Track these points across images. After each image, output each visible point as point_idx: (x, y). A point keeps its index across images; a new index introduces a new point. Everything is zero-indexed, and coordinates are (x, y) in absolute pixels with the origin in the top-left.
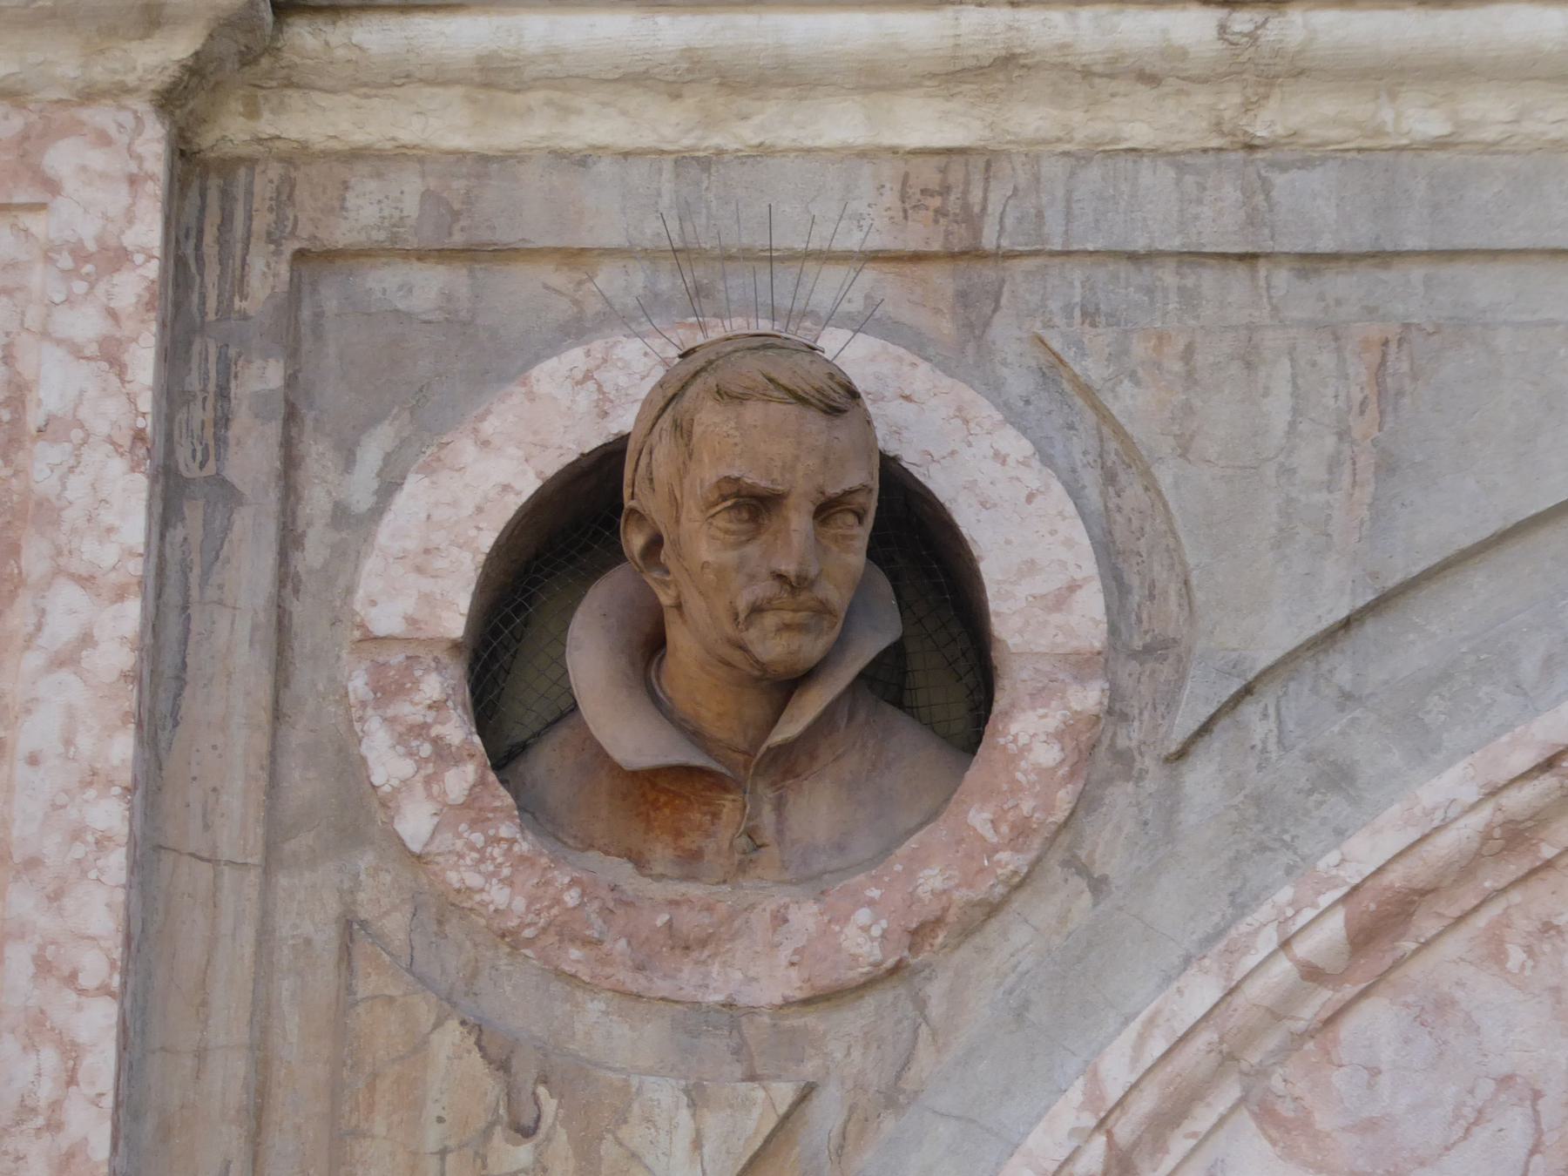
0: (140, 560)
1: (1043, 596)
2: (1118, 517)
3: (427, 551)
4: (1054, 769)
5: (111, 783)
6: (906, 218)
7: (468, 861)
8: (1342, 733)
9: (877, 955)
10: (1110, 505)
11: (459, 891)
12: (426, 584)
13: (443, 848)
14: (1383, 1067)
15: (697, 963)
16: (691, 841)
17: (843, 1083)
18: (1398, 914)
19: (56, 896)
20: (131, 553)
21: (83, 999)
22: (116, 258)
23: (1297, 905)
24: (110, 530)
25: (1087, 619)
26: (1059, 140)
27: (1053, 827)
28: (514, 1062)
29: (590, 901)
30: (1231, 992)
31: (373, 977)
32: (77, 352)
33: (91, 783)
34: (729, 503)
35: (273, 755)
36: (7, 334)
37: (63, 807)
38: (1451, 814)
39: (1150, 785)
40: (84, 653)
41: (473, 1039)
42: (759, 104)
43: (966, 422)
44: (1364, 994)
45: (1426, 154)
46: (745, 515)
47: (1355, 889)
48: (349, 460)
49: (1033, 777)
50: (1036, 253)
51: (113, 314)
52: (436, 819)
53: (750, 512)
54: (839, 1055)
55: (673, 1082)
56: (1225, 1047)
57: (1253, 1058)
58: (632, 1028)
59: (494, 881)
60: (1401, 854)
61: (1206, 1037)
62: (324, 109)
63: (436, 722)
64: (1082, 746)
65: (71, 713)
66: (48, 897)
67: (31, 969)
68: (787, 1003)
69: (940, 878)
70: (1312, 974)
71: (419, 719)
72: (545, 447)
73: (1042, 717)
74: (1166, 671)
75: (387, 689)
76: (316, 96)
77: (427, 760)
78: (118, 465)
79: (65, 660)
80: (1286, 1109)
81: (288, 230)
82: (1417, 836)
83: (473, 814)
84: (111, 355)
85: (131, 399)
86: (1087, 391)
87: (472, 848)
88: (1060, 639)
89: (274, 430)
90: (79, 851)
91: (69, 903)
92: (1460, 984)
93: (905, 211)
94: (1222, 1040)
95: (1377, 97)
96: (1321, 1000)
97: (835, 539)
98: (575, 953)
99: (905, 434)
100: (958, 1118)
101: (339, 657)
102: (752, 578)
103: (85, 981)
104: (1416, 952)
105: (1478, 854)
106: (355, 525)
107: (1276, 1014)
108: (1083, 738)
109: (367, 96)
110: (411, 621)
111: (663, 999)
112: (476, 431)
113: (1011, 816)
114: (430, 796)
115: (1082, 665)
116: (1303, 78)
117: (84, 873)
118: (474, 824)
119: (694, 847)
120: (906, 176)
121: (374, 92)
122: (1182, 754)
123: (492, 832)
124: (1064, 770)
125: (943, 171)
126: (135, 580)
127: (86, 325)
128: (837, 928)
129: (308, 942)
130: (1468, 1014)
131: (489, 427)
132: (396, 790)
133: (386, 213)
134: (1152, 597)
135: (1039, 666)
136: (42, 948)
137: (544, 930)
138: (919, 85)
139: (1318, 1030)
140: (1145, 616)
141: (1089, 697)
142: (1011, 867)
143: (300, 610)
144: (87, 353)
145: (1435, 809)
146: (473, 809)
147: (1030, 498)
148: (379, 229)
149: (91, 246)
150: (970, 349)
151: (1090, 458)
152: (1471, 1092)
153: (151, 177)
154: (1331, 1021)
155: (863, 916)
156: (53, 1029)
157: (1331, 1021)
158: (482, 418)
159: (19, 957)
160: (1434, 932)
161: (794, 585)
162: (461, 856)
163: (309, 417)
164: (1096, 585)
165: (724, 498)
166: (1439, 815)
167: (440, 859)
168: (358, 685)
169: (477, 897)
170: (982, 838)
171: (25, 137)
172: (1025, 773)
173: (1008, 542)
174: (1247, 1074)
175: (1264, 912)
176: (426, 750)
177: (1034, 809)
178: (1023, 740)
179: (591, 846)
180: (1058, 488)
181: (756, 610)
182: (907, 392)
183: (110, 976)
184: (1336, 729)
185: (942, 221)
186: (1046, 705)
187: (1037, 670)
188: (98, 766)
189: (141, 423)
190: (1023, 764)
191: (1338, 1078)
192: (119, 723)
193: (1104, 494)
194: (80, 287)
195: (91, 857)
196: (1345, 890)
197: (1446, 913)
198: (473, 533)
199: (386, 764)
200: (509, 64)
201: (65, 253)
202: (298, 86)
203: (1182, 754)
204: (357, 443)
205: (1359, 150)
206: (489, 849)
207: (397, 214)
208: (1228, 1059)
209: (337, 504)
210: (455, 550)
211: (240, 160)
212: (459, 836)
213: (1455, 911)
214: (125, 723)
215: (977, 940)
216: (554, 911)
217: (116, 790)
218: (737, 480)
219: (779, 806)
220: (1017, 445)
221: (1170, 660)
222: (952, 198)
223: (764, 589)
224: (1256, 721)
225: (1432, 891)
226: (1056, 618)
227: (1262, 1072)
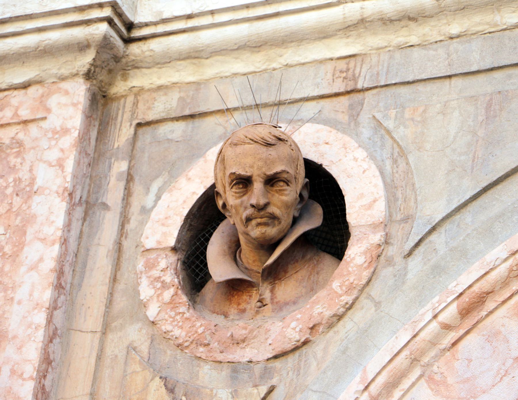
0: (61, 231)
1: (365, 205)
2: (397, 175)
3: (166, 218)
4: (362, 265)
5: (43, 307)
6: (333, 82)
7: (169, 322)
8: (464, 240)
9: (298, 338)
10: (394, 171)
11: (165, 333)
12: (165, 229)
13: (161, 318)
14: (473, 359)
15: (241, 348)
16: (243, 306)
17: (285, 385)
18: (478, 302)
19: (20, 348)
20: (58, 229)
21: (24, 382)
22: (65, 131)
23: (439, 302)
24: (53, 222)
25: (379, 211)
26: (386, 47)
27: (362, 286)
28: (176, 389)
29: (208, 330)
30: (415, 336)
31: (133, 365)
32: (50, 165)
33: (36, 308)
34: (234, 182)
35: (111, 294)
36: (32, 162)
37: (26, 317)
38: (497, 263)
39: (397, 267)
40: (40, 264)
41: (163, 383)
42: (285, 50)
43: (346, 148)
44: (467, 333)
45: (514, 30)
46: (241, 186)
47: (461, 294)
48: (148, 190)
49: (355, 269)
50: (376, 87)
51: (62, 150)
52: (160, 309)
53: (243, 185)
54: (285, 375)
55: (227, 390)
56: (413, 357)
57: (426, 360)
58: (218, 373)
59: (176, 327)
60: (478, 280)
61: (405, 353)
62: (146, 74)
63: (164, 276)
64: (373, 256)
65: (33, 285)
66: (18, 349)
67: (9, 373)
68: (268, 360)
69: (321, 308)
70: (447, 327)
71: (158, 275)
72: (208, 177)
73: (360, 247)
74: (407, 226)
75: (150, 266)
76: (144, 70)
77: (159, 289)
78: (58, 200)
79: (33, 268)
80: (437, 377)
81: (135, 117)
82: (483, 272)
83: (172, 306)
84: (60, 164)
85: (65, 178)
86: (388, 132)
87: (171, 317)
88: (369, 219)
89: (122, 185)
90: (29, 331)
91: (24, 349)
92: (503, 325)
93: (333, 80)
94: (411, 354)
95: (494, 12)
96: (452, 336)
97: (277, 191)
98: (201, 349)
99: (325, 156)
100: (319, 392)
101: (137, 258)
102: (246, 208)
103: (25, 376)
104: (487, 316)
105: (508, 277)
106: (145, 211)
107: (433, 343)
108: (374, 253)
109: (160, 68)
110: (159, 242)
111: (228, 362)
112: (187, 175)
113: (347, 283)
114: (158, 301)
115: (374, 227)
116: (466, 10)
117: (30, 338)
118: (172, 309)
119: (243, 308)
120: (335, 67)
121: (162, 66)
122: (410, 254)
123: (177, 311)
124: (366, 264)
125: (348, 64)
126: (58, 238)
127: (53, 155)
128: (285, 330)
129: (116, 356)
130: (505, 336)
131: (190, 174)
132: (148, 300)
133: (166, 107)
134: (405, 201)
135: (361, 230)
136: (13, 366)
137: (192, 343)
138: (336, 35)
139: (450, 348)
140: (402, 208)
141: (377, 238)
142: (345, 301)
143: (126, 244)
144: (53, 164)
145: (491, 262)
146: (172, 304)
147: (364, 172)
148: (163, 112)
149: (58, 129)
150: (352, 124)
151: (389, 156)
152: (504, 364)
153: (80, 103)
154: (454, 344)
155: (293, 324)
156: (13, 393)
157: (454, 344)
158: (189, 171)
159: (6, 370)
160: (493, 307)
161: (260, 208)
162: (167, 320)
163: (137, 178)
164: (383, 199)
165: (233, 181)
166: (492, 264)
167: (160, 322)
168: (140, 266)
169: (171, 334)
170: (336, 292)
171: (43, 96)
172: (352, 267)
173: (355, 188)
174: (424, 366)
175: (429, 306)
176: (159, 285)
177: (354, 280)
178: (352, 256)
179: (214, 313)
180: (374, 167)
181: (249, 220)
182: (327, 142)
183: (33, 373)
184: (461, 238)
185: (345, 80)
186: (362, 243)
187: (360, 232)
188: (39, 302)
189: (66, 185)
190: (352, 265)
191: (457, 364)
192: (47, 286)
193: (392, 168)
194: (53, 143)
195: (33, 333)
196: (458, 294)
197: (498, 300)
198: (181, 210)
199: (146, 291)
200: (201, 49)
201: (50, 133)
202: (137, 68)
203: (410, 254)
204: (150, 185)
205: (490, 33)
206: (176, 317)
207: (170, 107)
208: (414, 361)
209: (142, 207)
210: (175, 216)
211: (123, 96)
212: (167, 313)
213: (502, 299)
214: (49, 286)
215: (335, 329)
216: (195, 336)
217: (44, 309)
218: (234, 173)
219: (272, 291)
220: (361, 154)
221: (409, 223)
222: (349, 73)
223: (250, 211)
224: (438, 239)
225: (492, 292)
226: (369, 212)
227: (428, 365)
